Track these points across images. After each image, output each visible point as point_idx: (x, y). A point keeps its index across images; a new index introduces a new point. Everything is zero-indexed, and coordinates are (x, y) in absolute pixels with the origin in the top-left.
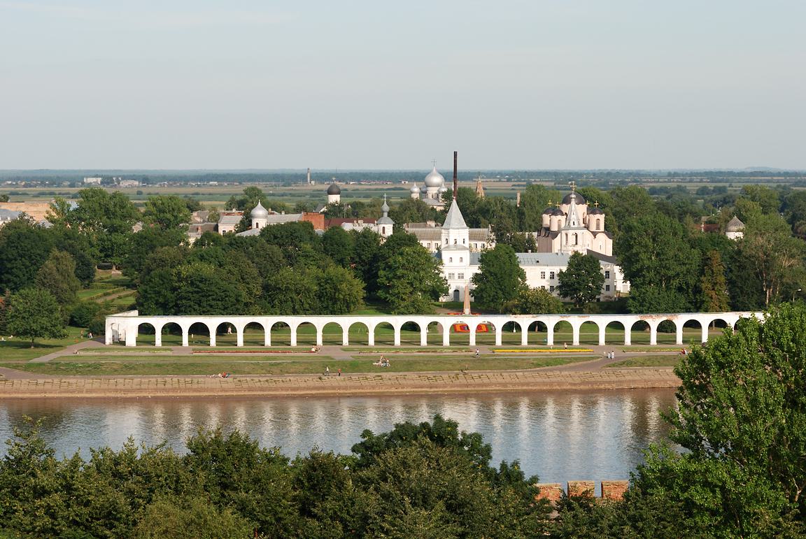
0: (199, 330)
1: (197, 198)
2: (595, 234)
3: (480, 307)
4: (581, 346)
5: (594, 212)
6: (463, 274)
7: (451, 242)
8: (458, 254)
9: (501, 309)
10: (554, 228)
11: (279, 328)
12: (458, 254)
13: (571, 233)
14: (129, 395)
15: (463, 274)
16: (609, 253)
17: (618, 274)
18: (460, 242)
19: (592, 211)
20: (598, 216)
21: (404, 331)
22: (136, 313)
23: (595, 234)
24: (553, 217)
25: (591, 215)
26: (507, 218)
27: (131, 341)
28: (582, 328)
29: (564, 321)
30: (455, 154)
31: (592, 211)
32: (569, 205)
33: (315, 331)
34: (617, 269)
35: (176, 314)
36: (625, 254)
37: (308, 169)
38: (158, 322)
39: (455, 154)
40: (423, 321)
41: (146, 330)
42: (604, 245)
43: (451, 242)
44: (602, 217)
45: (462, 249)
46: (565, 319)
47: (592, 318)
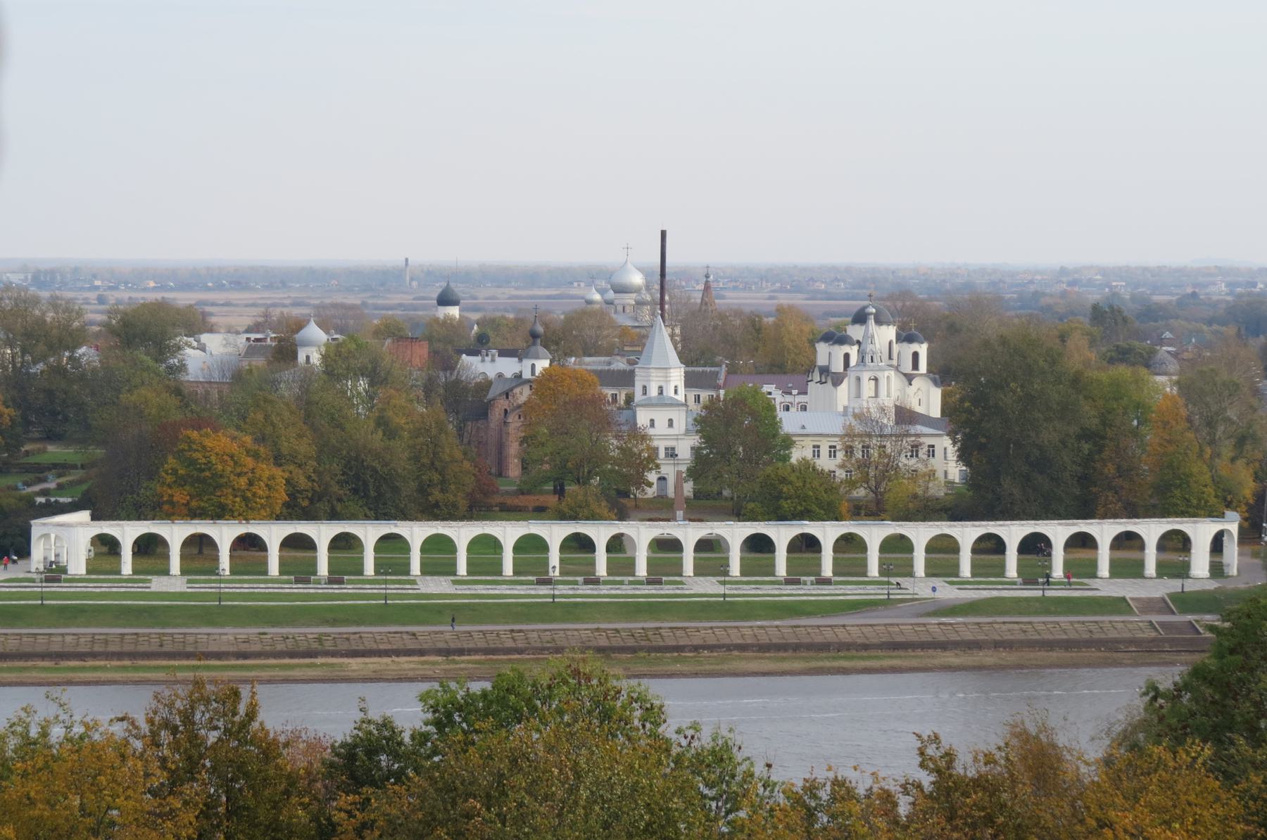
0: (200, 547)
1: (208, 309)
2: (909, 378)
3: (703, 505)
4: (611, 578)
5: (910, 339)
6: (673, 449)
7: (653, 392)
8: (666, 407)
9: (844, 507)
10: (838, 367)
11: (343, 543)
12: (666, 407)
13: (865, 376)
14: (307, 661)
15: (673, 449)
16: (936, 412)
17: (946, 446)
18: (670, 392)
19: (905, 337)
20: (915, 347)
21: (239, 553)
22: (84, 516)
23: (909, 378)
24: (836, 347)
25: (905, 345)
26: (750, 347)
27: (77, 566)
28: (930, 549)
29: (347, 534)
30: (663, 234)
31: (905, 337)
32: (863, 327)
33: (1142, 547)
34: (946, 442)
35: (1182, 514)
36: (958, 417)
37: (407, 260)
38: (127, 532)
39: (663, 234)
40: (600, 533)
41: (107, 545)
42: (928, 399)
43: (653, 392)
44: (923, 349)
45: (671, 405)
46: (947, 531)
47: (108, 528)
